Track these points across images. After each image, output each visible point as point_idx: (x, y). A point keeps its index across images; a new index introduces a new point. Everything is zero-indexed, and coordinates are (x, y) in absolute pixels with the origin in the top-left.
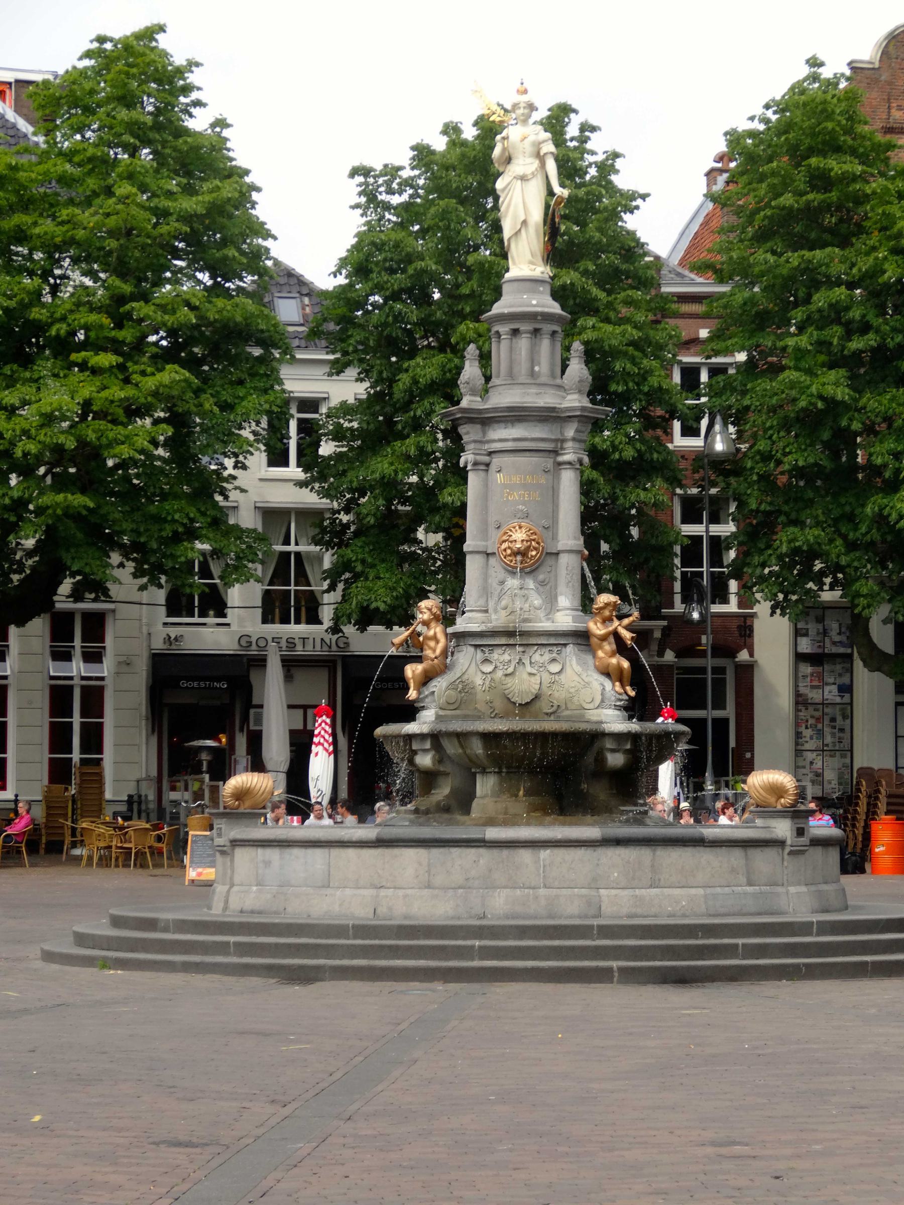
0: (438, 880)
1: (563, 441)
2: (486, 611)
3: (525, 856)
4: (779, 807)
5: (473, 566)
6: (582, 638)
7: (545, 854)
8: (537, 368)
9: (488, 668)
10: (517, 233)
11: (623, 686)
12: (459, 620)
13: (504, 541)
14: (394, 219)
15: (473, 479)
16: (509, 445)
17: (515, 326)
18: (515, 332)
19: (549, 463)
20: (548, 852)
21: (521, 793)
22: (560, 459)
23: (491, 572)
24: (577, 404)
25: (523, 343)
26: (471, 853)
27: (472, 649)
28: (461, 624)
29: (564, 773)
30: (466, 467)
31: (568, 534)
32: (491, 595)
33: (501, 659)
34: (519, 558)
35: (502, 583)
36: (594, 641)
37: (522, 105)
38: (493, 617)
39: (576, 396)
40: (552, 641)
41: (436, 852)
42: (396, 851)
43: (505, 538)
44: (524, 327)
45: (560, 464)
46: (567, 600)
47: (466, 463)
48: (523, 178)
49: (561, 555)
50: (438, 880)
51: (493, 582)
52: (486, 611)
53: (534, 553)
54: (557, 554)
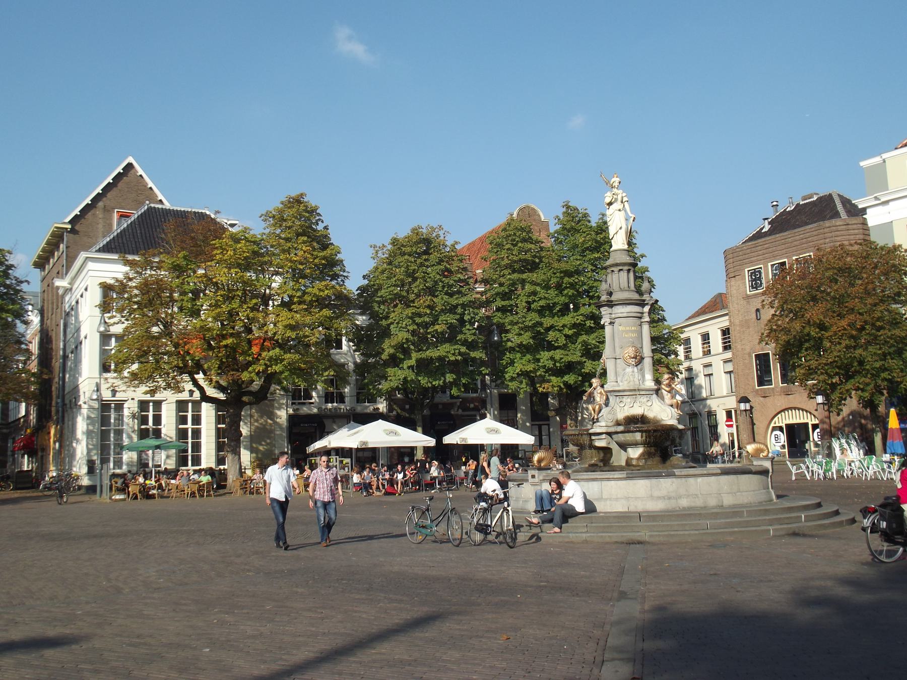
1: (642, 313)
3: (691, 480)
7: (700, 480)
15: (608, 330)
18: (620, 270)
19: (637, 321)
23: (618, 366)
25: (624, 275)
28: (607, 387)
44: (626, 268)
46: (649, 376)
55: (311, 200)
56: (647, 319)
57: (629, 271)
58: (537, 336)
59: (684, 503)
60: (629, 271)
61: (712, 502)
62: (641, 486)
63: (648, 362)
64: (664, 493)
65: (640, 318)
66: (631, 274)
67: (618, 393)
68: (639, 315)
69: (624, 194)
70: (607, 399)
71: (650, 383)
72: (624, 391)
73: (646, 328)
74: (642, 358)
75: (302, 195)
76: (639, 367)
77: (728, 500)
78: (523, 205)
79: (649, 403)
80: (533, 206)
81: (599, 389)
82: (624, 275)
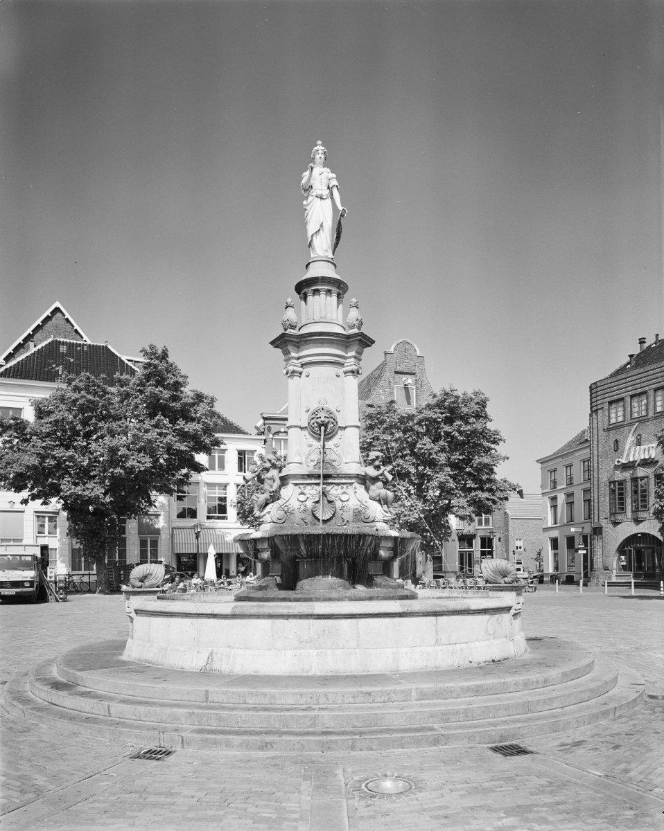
13: (313, 419)
49: (347, 429)
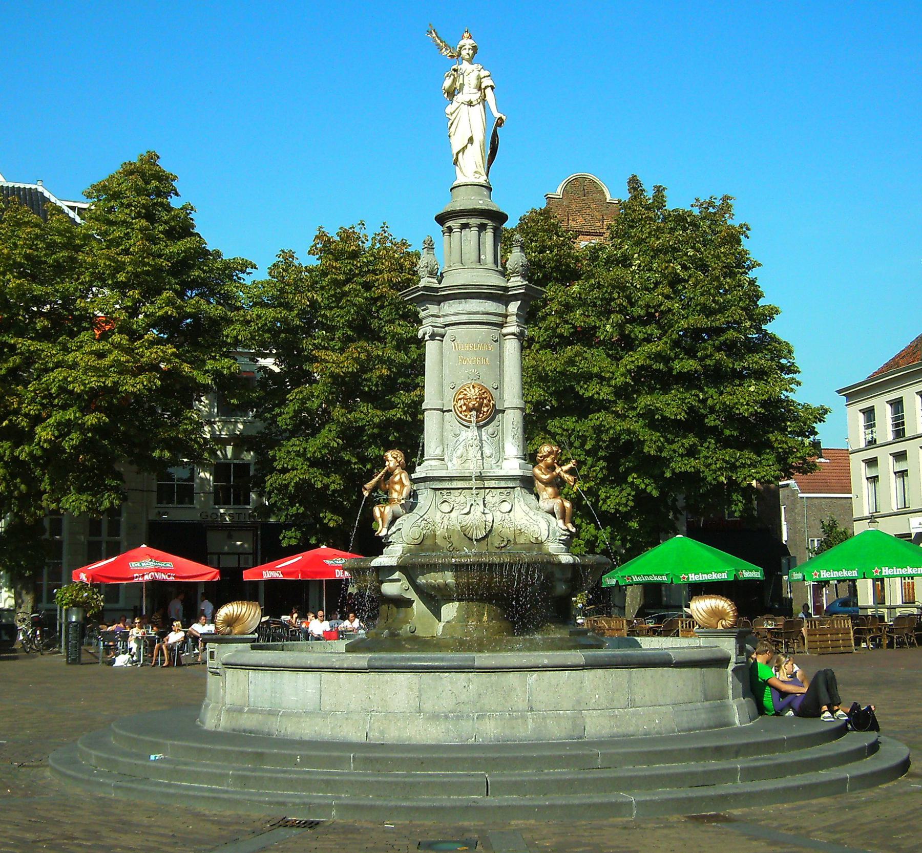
0: (428, 706)
1: (506, 316)
2: (443, 460)
3: (512, 678)
4: (720, 627)
5: (431, 421)
6: (528, 483)
7: (532, 678)
8: (482, 257)
9: (446, 507)
10: (463, 149)
11: (565, 523)
12: (418, 468)
14: (229, 455)
15: (431, 347)
16: (464, 318)
17: (464, 221)
18: (465, 226)
19: (494, 332)
20: (535, 675)
21: (485, 618)
22: (505, 331)
23: (447, 426)
24: (520, 284)
25: (471, 235)
26: (461, 678)
27: (431, 492)
28: (420, 472)
29: (523, 601)
30: (423, 337)
31: (511, 395)
32: (448, 444)
33: (458, 500)
34: (474, 413)
35: (456, 435)
36: (538, 484)
37: (467, 47)
38: (449, 464)
39: (519, 278)
40: (503, 484)
41: (426, 677)
42: (388, 676)
43: (461, 396)
44: (474, 221)
45: (505, 335)
46: (512, 448)
47: (424, 334)
48: (470, 104)
50: (428, 706)
51: (449, 435)
52: (443, 460)
53: (485, 409)
54: (503, 411)
55: (165, 165)
56: (514, 329)
57: (482, 228)
58: (801, 431)
59: (490, 730)
60: (482, 228)
61: (557, 730)
62: (453, 689)
63: (512, 421)
64: (446, 704)
65: (501, 326)
66: (489, 236)
67: (441, 484)
68: (499, 320)
69: (484, 73)
70: (413, 495)
71: (513, 465)
72: (451, 479)
73: (511, 347)
74: (496, 412)
75: (152, 158)
76: (490, 428)
77: (596, 725)
78: (572, 176)
79: (506, 507)
80: (592, 177)
81: (400, 476)
82: (471, 235)
